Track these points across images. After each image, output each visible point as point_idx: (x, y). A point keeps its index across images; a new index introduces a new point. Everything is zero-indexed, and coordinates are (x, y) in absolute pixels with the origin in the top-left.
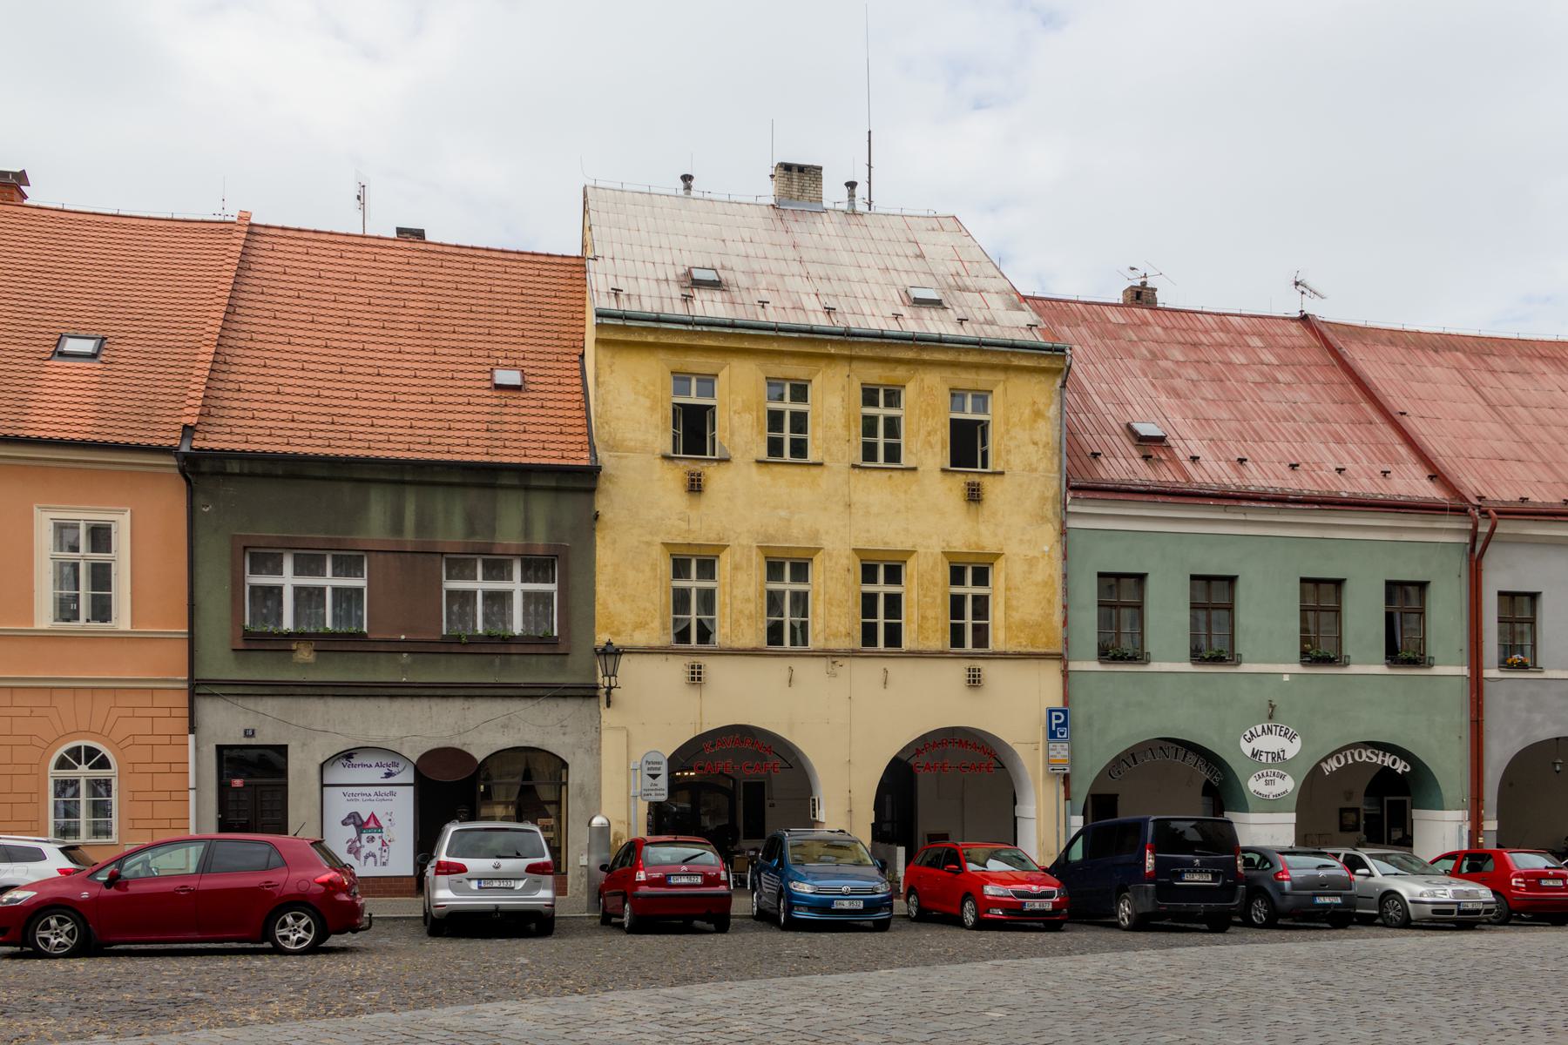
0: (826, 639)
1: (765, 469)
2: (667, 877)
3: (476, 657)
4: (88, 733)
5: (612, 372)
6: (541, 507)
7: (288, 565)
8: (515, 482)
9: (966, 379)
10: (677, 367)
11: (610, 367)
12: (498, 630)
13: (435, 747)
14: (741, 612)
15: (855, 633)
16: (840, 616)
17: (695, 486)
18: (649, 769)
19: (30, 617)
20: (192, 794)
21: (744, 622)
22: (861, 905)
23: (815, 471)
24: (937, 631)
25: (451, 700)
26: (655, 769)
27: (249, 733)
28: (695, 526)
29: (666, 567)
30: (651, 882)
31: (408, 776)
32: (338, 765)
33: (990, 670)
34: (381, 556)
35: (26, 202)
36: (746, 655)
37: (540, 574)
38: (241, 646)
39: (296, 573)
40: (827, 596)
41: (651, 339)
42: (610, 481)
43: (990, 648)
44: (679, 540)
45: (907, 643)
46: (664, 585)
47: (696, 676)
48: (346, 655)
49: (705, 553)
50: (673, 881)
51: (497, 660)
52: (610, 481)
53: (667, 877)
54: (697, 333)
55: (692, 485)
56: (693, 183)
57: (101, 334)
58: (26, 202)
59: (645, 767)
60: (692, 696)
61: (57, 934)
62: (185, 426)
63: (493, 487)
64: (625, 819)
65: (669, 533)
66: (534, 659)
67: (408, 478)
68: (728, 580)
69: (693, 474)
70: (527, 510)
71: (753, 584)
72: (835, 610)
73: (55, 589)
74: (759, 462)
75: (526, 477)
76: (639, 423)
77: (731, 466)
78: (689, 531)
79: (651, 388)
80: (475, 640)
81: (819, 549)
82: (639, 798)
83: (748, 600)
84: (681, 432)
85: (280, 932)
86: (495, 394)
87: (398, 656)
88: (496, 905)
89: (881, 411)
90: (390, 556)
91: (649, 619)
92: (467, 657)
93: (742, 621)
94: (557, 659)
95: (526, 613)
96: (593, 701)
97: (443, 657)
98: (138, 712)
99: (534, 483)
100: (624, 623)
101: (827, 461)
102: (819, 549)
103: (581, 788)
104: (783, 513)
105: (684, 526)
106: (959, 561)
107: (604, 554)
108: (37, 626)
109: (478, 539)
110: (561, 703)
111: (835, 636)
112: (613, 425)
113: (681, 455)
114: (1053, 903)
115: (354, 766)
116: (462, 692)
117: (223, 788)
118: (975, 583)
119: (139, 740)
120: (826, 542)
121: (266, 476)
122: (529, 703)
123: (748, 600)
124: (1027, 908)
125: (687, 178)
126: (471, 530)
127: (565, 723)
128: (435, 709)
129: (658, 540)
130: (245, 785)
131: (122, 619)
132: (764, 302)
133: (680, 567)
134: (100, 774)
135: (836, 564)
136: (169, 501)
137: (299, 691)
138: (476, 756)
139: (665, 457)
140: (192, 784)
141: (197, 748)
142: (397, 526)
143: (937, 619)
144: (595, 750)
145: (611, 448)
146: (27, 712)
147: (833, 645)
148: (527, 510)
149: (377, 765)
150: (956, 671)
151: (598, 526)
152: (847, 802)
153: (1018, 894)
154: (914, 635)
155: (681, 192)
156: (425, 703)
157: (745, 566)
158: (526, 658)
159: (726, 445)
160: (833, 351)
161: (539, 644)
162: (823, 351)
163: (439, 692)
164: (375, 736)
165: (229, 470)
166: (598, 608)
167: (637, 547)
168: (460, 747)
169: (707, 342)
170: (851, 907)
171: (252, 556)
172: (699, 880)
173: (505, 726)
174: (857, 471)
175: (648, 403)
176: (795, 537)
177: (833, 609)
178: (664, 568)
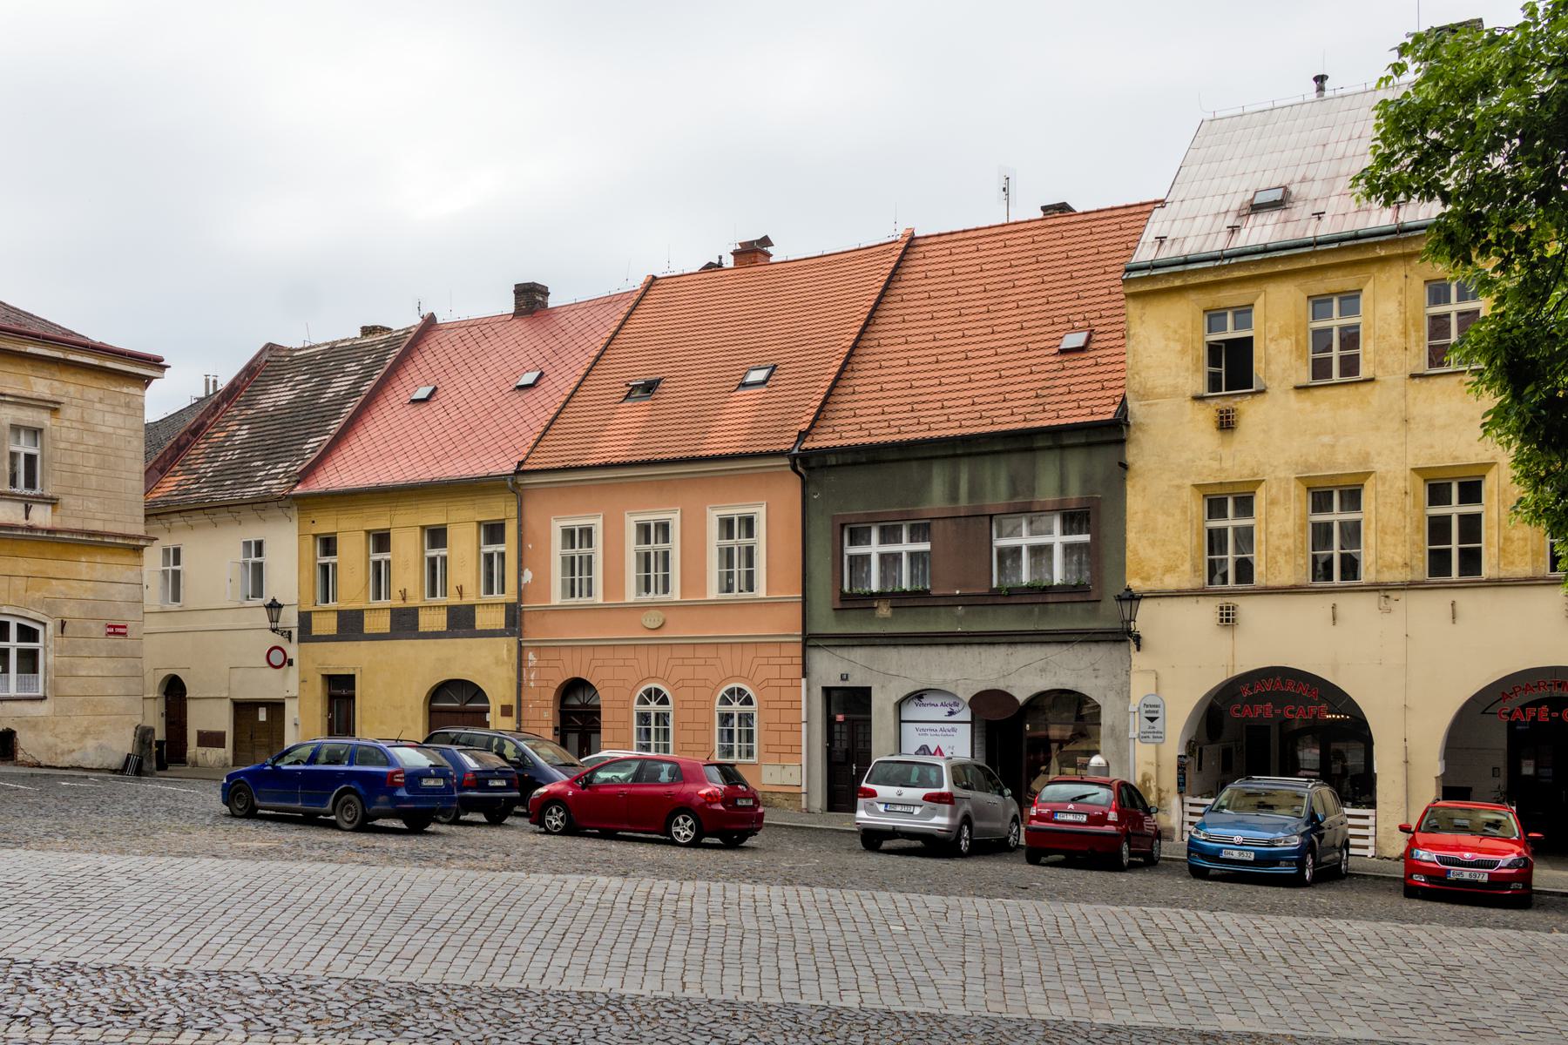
0: (1378, 572)
1: (1305, 395)
2: (1053, 813)
3: (1019, 607)
4: (739, 677)
5: (1143, 322)
6: (1076, 464)
7: (875, 535)
8: (1049, 443)
9: (1320, 285)
10: (1209, 305)
11: (1141, 318)
12: (1010, 582)
13: (984, 689)
14: (1278, 549)
15: (1414, 562)
16: (1395, 545)
17: (1226, 423)
18: (1146, 712)
19: (704, 593)
20: (804, 725)
21: (1281, 559)
22: (1252, 857)
23: (1367, 387)
24: (1526, 553)
25: (996, 646)
26: (1154, 712)
27: (844, 677)
28: (1227, 464)
29: (1198, 508)
30: (1040, 817)
31: (966, 715)
32: (912, 704)
33: (1248, 608)
34: (941, 522)
35: (772, 260)
36: (1283, 593)
37: (1075, 525)
38: (838, 606)
39: (1064, 533)
40: (1380, 524)
41: (1178, 283)
42: (1140, 429)
43: (1483, 575)
44: (1211, 480)
45: (1488, 569)
46: (1195, 526)
47: (1224, 617)
48: (914, 610)
49: (1239, 490)
50: (1059, 817)
51: (1036, 609)
52: (1140, 429)
53: (1053, 813)
54: (1224, 267)
55: (1222, 423)
56: (1327, 84)
57: (770, 364)
58: (772, 260)
59: (1143, 710)
60: (1223, 638)
61: (555, 819)
62: (800, 432)
63: (1032, 450)
64: (1154, 761)
65: (1200, 474)
66: (1069, 607)
67: (959, 451)
68: (1263, 516)
69: (1221, 412)
70: (1062, 467)
71: (1291, 517)
72: (1390, 539)
73: (720, 567)
74: (1297, 388)
75: (1057, 438)
76: (1170, 368)
77: (1267, 397)
78: (1221, 470)
79: (1181, 331)
80: (995, 593)
81: (1370, 473)
82: (1137, 740)
83: (1286, 536)
84: (1223, 369)
85: (675, 829)
86: (1059, 359)
87: (954, 609)
88: (894, 827)
89: (1336, 322)
90: (948, 521)
91: (1179, 563)
92: (1010, 608)
93: (1279, 558)
94: (1089, 606)
95: (1066, 564)
96: (1124, 645)
97: (989, 608)
98: (772, 661)
99: (1067, 441)
100: (1154, 568)
101: (1380, 375)
102: (1370, 473)
103: (1113, 729)
104: (1326, 439)
105: (1215, 465)
106: (1440, 477)
107: (1136, 502)
108: (627, 601)
109: (1019, 500)
110: (1094, 647)
111: (1390, 567)
112: (1143, 374)
113: (1224, 393)
114: (1490, 874)
115: (924, 705)
116: (1004, 639)
117: (830, 722)
118: (1462, 501)
119: (772, 683)
120: (1378, 466)
121: (855, 464)
122: (1065, 647)
123: (1286, 536)
124: (1452, 877)
125: (1320, 79)
126: (1014, 493)
127: (1096, 666)
128: (983, 655)
129: (1188, 482)
130: (846, 719)
131: (761, 591)
132: (1318, 214)
133: (1216, 507)
134: (662, 708)
135: (1391, 487)
136: (790, 490)
137: (878, 641)
138: (1018, 698)
139: (1198, 398)
140: (804, 719)
141: (808, 690)
142: (954, 496)
143: (1525, 539)
144: (1124, 692)
145: (1143, 396)
146: (702, 661)
147: (1387, 577)
148: (1062, 467)
149: (942, 704)
150: (1208, 610)
151: (1129, 475)
152: (1404, 750)
153: (1443, 860)
154: (1494, 561)
155: (1314, 96)
156: (975, 650)
157: (1282, 498)
158: (1062, 607)
159: (1261, 376)
160: (1383, 253)
161: (1074, 592)
162: (1371, 255)
163: (987, 640)
164: (935, 679)
165: (829, 463)
166: (1129, 554)
167: (1167, 492)
168: (1004, 689)
169: (1237, 274)
170: (1241, 858)
171: (852, 531)
172: (1084, 818)
173: (1043, 670)
174: (1417, 381)
175: (1178, 347)
176: (1342, 463)
177: (1387, 537)
178: (1195, 509)
